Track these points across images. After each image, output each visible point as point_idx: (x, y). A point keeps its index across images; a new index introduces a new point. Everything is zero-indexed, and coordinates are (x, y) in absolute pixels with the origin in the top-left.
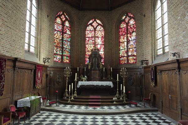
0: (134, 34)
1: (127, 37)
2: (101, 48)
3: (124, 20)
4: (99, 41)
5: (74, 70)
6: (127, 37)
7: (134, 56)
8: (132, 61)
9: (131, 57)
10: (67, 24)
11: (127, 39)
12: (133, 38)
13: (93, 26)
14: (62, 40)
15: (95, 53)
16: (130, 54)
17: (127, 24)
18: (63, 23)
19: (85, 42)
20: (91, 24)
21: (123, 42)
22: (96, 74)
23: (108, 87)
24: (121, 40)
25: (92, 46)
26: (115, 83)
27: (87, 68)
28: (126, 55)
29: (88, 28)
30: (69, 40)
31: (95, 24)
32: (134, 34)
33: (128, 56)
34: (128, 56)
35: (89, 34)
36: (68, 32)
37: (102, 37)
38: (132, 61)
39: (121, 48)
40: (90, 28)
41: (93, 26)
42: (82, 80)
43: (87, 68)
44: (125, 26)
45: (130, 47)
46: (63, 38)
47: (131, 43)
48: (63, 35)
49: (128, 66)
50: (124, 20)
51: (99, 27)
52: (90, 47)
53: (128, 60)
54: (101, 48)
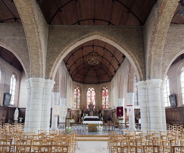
0: (108, 96)
3: (104, 89)
4: (93, 98)
5: (83, 111)
7: (108, 105)
8: (107, 108)
10: (79, 91)
11: (105, 98)
13: (90, 91)
14: (77, 98)
15: (91, 105)
16: (106, 104)
17: (105, 91)
20: (89, 90)
22: (92, 113)
24: (103, 98)
26: (99, 117)
27: (88, 111)
30: (79, 98)
31: (91, 90)
32: (108, 96)
33: (106, 105)
35: (88, 94)
36: (79, 94)
39: (103, 102)
40: (89, 92)
41: (90, 91)
43: (88, 111)
46: (77, 97)
47: (107, 100)
49: (105, 110)
50: (104, 89)
52: (89, 101)
53: (105, 107)
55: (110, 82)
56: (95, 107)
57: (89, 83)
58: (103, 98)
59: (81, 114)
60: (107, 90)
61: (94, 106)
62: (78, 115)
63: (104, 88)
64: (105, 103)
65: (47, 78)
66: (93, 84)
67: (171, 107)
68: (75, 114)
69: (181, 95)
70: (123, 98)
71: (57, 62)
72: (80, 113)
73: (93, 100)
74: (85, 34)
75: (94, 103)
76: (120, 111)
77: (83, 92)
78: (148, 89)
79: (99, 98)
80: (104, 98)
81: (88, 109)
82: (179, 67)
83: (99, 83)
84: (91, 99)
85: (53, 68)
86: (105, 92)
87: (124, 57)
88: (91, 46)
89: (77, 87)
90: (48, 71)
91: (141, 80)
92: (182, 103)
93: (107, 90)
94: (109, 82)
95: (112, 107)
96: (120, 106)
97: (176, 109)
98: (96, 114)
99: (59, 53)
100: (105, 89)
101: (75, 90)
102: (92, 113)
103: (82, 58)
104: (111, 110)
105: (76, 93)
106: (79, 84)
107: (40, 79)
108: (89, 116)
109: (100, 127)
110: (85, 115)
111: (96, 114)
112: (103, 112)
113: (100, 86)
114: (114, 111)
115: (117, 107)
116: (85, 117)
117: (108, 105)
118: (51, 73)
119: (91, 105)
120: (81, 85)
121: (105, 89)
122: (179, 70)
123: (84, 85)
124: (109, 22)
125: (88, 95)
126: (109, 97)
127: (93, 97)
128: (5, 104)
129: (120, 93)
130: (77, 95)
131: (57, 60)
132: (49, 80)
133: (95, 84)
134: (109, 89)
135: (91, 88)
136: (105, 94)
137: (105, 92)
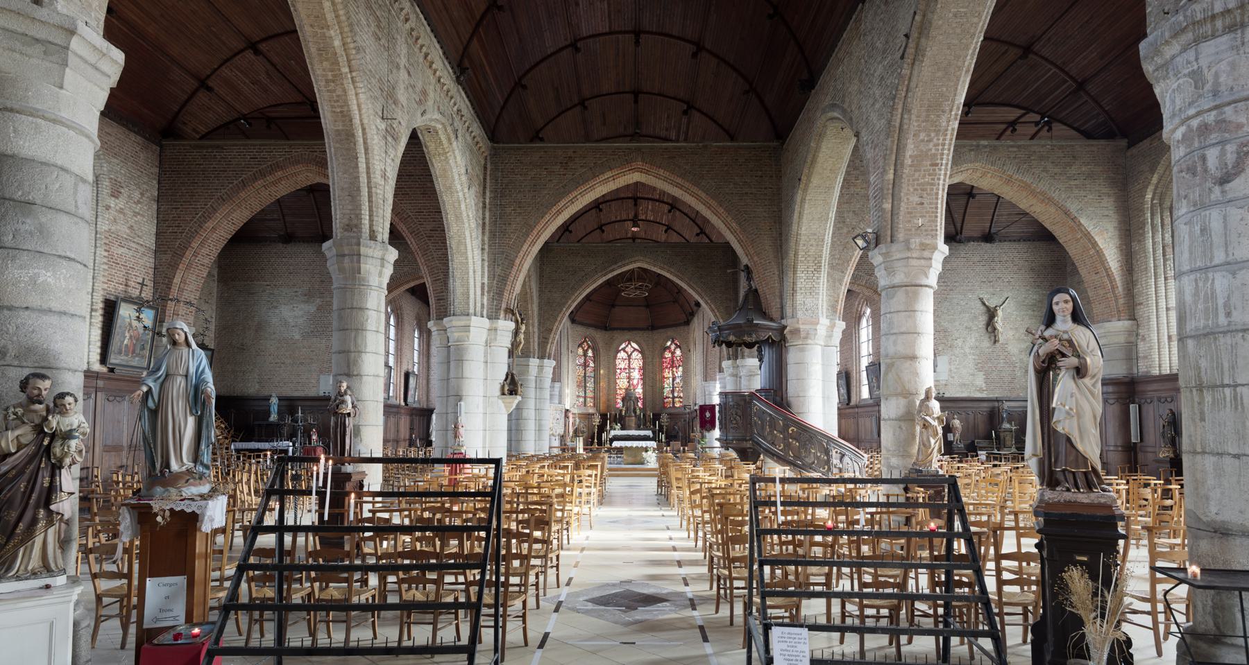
0: (681, 369)
1: (673, 372)
2: (638, 384)
3: (669, 348)
4: (636, 375)
5: (604, 417)
6: (673, 372)
7: (680, 397)
8: (677, 405)
9: (677, 399)
10: (590, 353)
11: (673, 374)
12: (680, 373)
13: (627, 353)
14: (585, 376)
15: (628, 398)
16: (676, 395)
17: (673, 353)
18: (585, 354)
19: (615, 375)
20: (624, 349)
21: (668, 378)
22: (632, 421)
23: (866, 588)
24: (666, 374)
25: (626, 381)
26: (654, 433)
27: (620, 414)
28: (671, 396)
29: (619, 355)
30: (592, 375)
31: (629, 349)
32: (681, 369)
33: (674, 398)
34: (674, 398)
35: (621, 364)
36: (592, 365)
37: (640, 369)
38: (677, 405)
39: (666, 386)
40: (622, 355)
41: (627, 353)
42: (615, 429)
43: (620, 414)
44: (670, 355)
45: (676, 385)
46: (585, 373)
47: (678, 380)
48: (585, 369)
49: (673, 411)
50: (669, 348)
51: (636, 353)
52: (622, 383)
53: (674, 403)
54: (638, 384)
55: (686, 328)
56: (644, 404)
57: (623, 329)
58: (668, 374)
59: (597, 424)
60: (678, 352)
61: (637, 399)
62: (591, 427)
63: (669, 343)
64: (673, 391)
65: (542, 357)
66: (635, 332)
67: (871, 401)
68: (582, 425)
69: (860, 376)
70: (715, 380)
71: (560, 322)
72: (597, 421)
73: (635, 382)
74: (616, 263)
75: (639, 391)
76: (708, 415)
77: (603, 358)
78: (740, 377)
79: (651, 375)
80: (671, 375)
81: (621, 411)
82: (857, 303)
83: (653, 328)
84: (629, 378)
85: (552, 336)
86: (673, 356)
87: (698, 304)
88: (630, 220)
89: (585, 341)
90: (543, 342)
91: (729, 359)
92: (860, 396)
93: (678, 352)
94: (682, 327)
95: (691, 404)
96: (707, 404)
97: (848, 411)
98: (645, 425)
99: (564, 304)
100: (673, 347)
101: (580, 351)
102: (632, 421)
103: (578, 109)
104: (688, 410)
105: (582, 361)
106: (591, 332)
107: (531, 360)
108: (623, 428)
109: (649, 453)
110: (612, 428)
111: (645, 425)
112: (664, 419)
113: (657, 335)
114: (694, 414)
115: (701, 406)
116: (613, 433)
117: (680, 397)
118: (549, 347)
119: (628, 398)
120: (599, 335)
121: (673, 347)
122: (857, 310)
123: (607, 334)
124: (687, 103)
125: (620, 367)
126: (684, 372)
127: (637, 371)
128: (410, 399)
129: (709, 367)
130: (585, 365)
131: (559, 319)
132: (546, 361)
133: (641, 332)
134: (684, 347)
135: (629, 343)
136: (673, 362)
137: (673, 356)
